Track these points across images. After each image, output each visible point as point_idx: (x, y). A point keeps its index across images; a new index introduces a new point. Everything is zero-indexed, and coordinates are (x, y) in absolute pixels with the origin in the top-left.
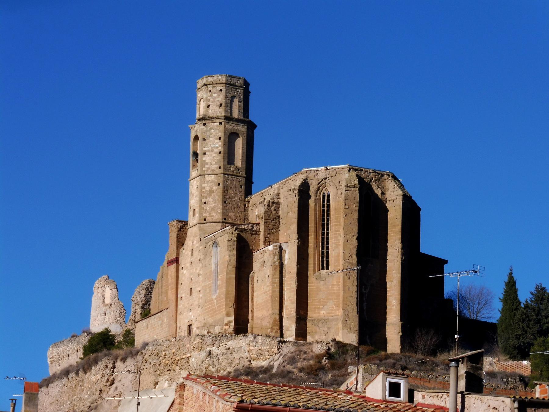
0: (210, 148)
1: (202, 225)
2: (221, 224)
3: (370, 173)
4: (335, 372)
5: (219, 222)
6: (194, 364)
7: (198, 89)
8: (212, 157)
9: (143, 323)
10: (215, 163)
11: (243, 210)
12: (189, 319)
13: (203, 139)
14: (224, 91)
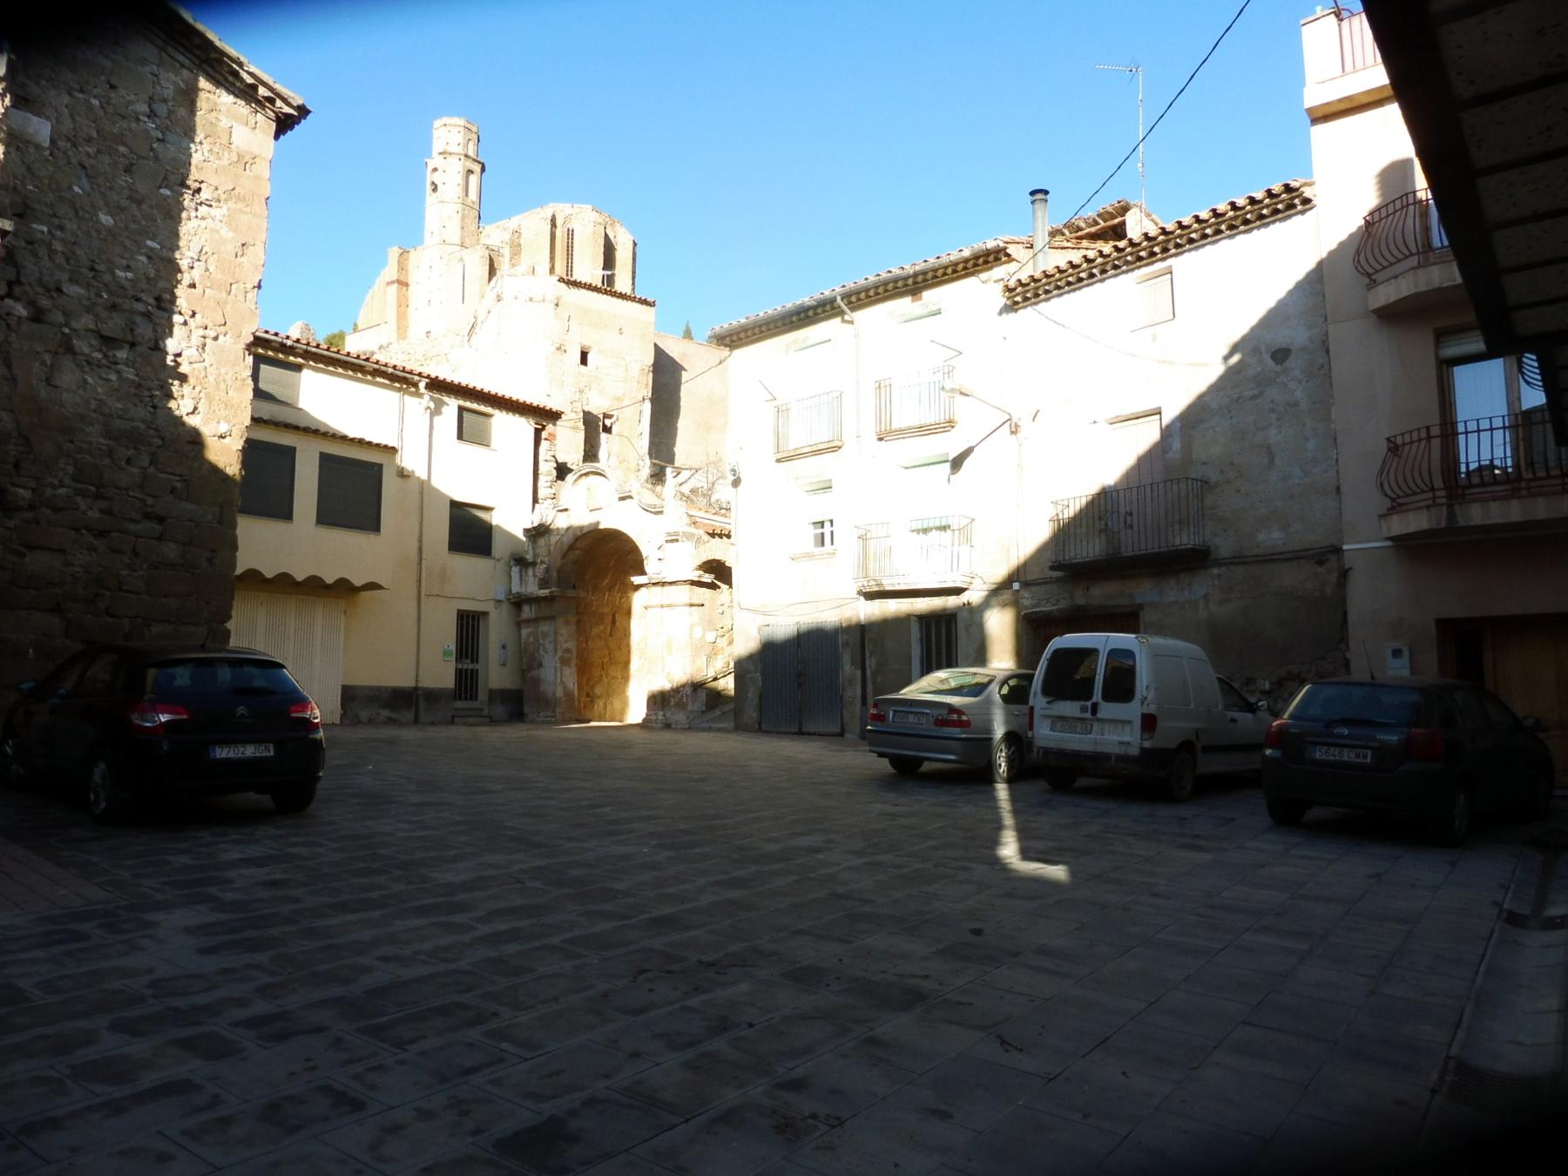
4: (1003, 764)
5: (458, 245)
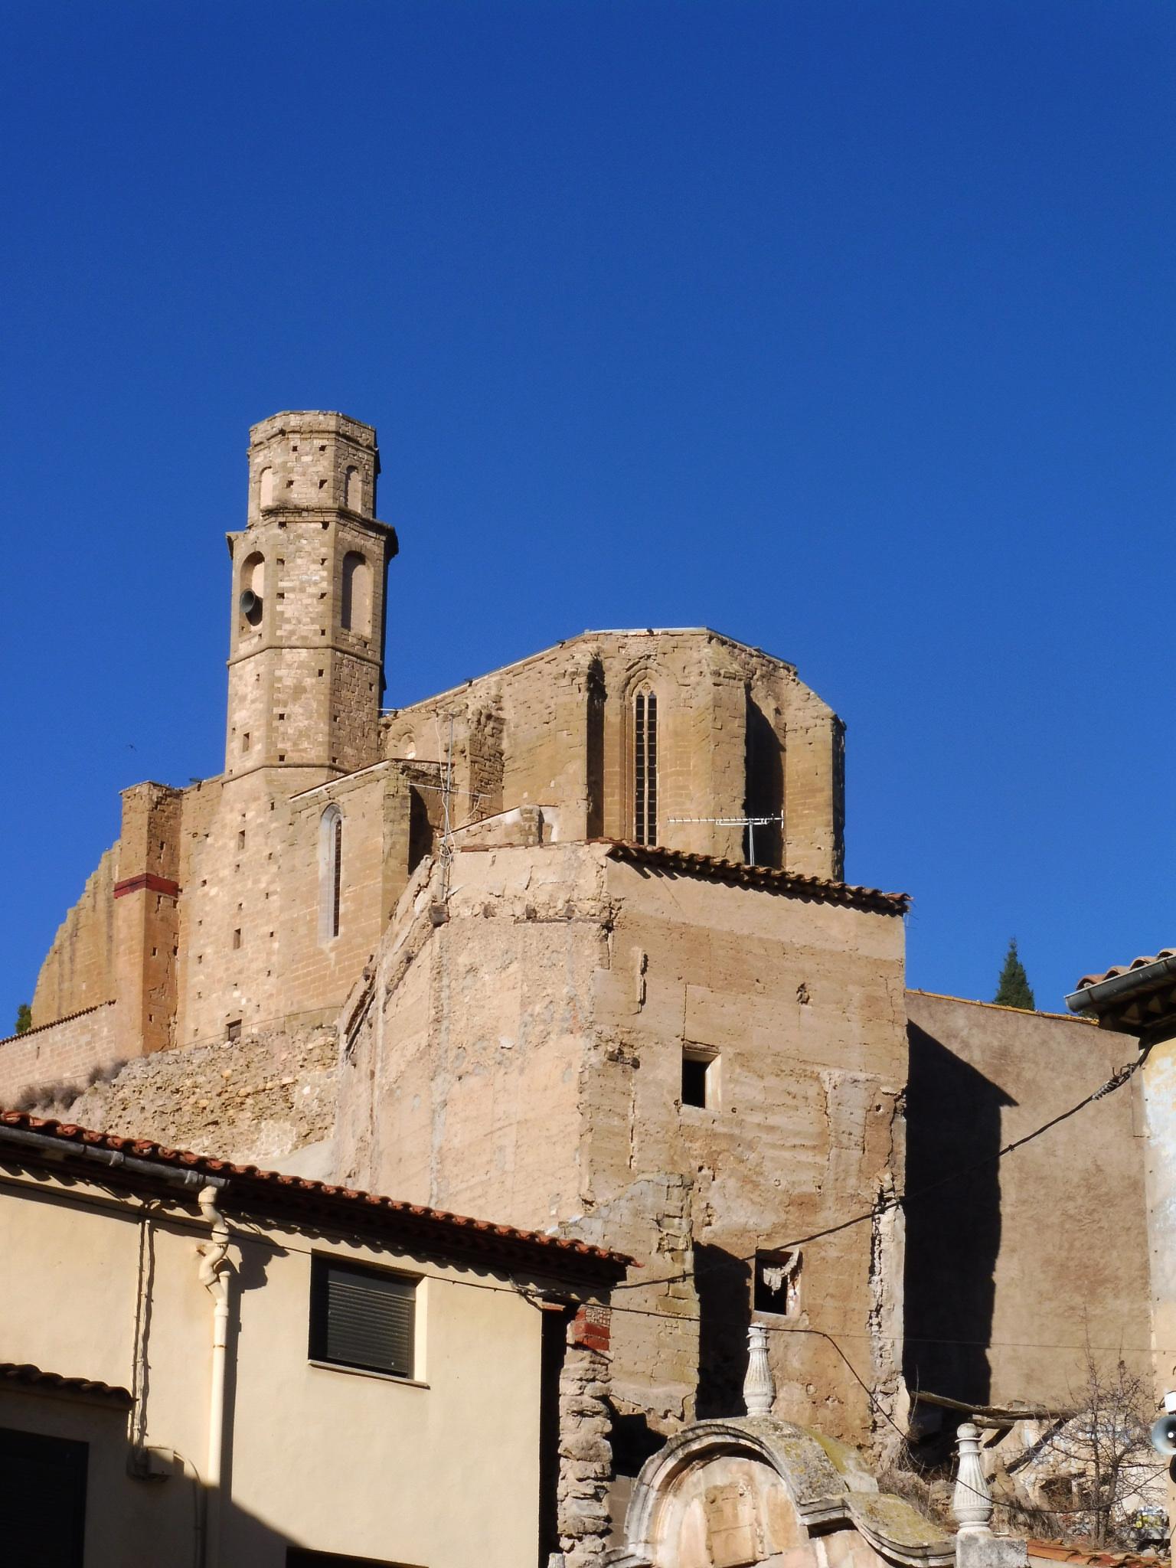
0: (298, 583)
1: (273, 771)
2: (325, 771)
3: (752, 656)
6: (309, 1101)
7: (256, 446)
8: (302, 605)
9: (25, 1043)
10: (309, 620)
11: (375, 746)
12: (230, 1008)
13: (278, 560)
14: (330, 452)
